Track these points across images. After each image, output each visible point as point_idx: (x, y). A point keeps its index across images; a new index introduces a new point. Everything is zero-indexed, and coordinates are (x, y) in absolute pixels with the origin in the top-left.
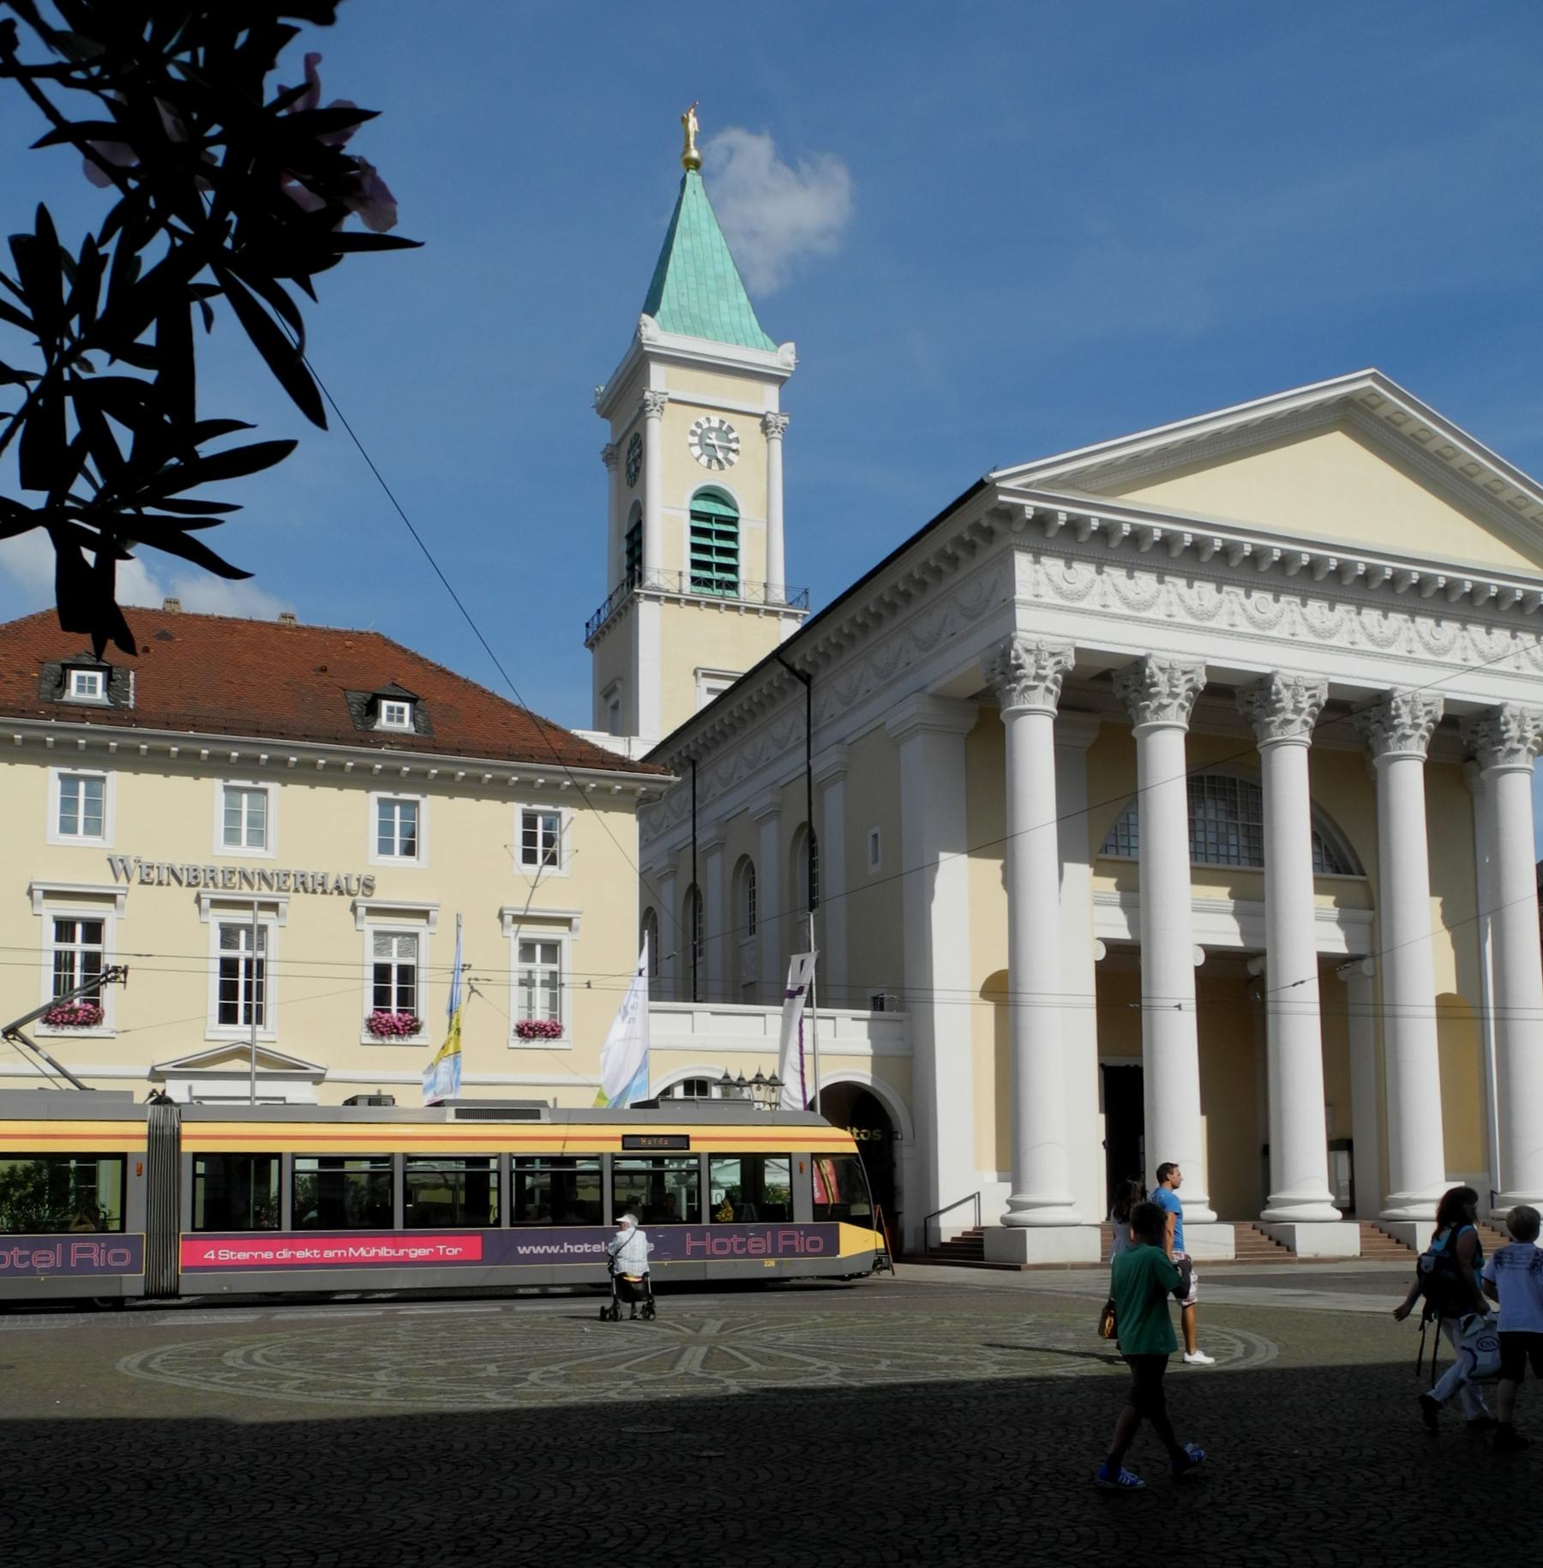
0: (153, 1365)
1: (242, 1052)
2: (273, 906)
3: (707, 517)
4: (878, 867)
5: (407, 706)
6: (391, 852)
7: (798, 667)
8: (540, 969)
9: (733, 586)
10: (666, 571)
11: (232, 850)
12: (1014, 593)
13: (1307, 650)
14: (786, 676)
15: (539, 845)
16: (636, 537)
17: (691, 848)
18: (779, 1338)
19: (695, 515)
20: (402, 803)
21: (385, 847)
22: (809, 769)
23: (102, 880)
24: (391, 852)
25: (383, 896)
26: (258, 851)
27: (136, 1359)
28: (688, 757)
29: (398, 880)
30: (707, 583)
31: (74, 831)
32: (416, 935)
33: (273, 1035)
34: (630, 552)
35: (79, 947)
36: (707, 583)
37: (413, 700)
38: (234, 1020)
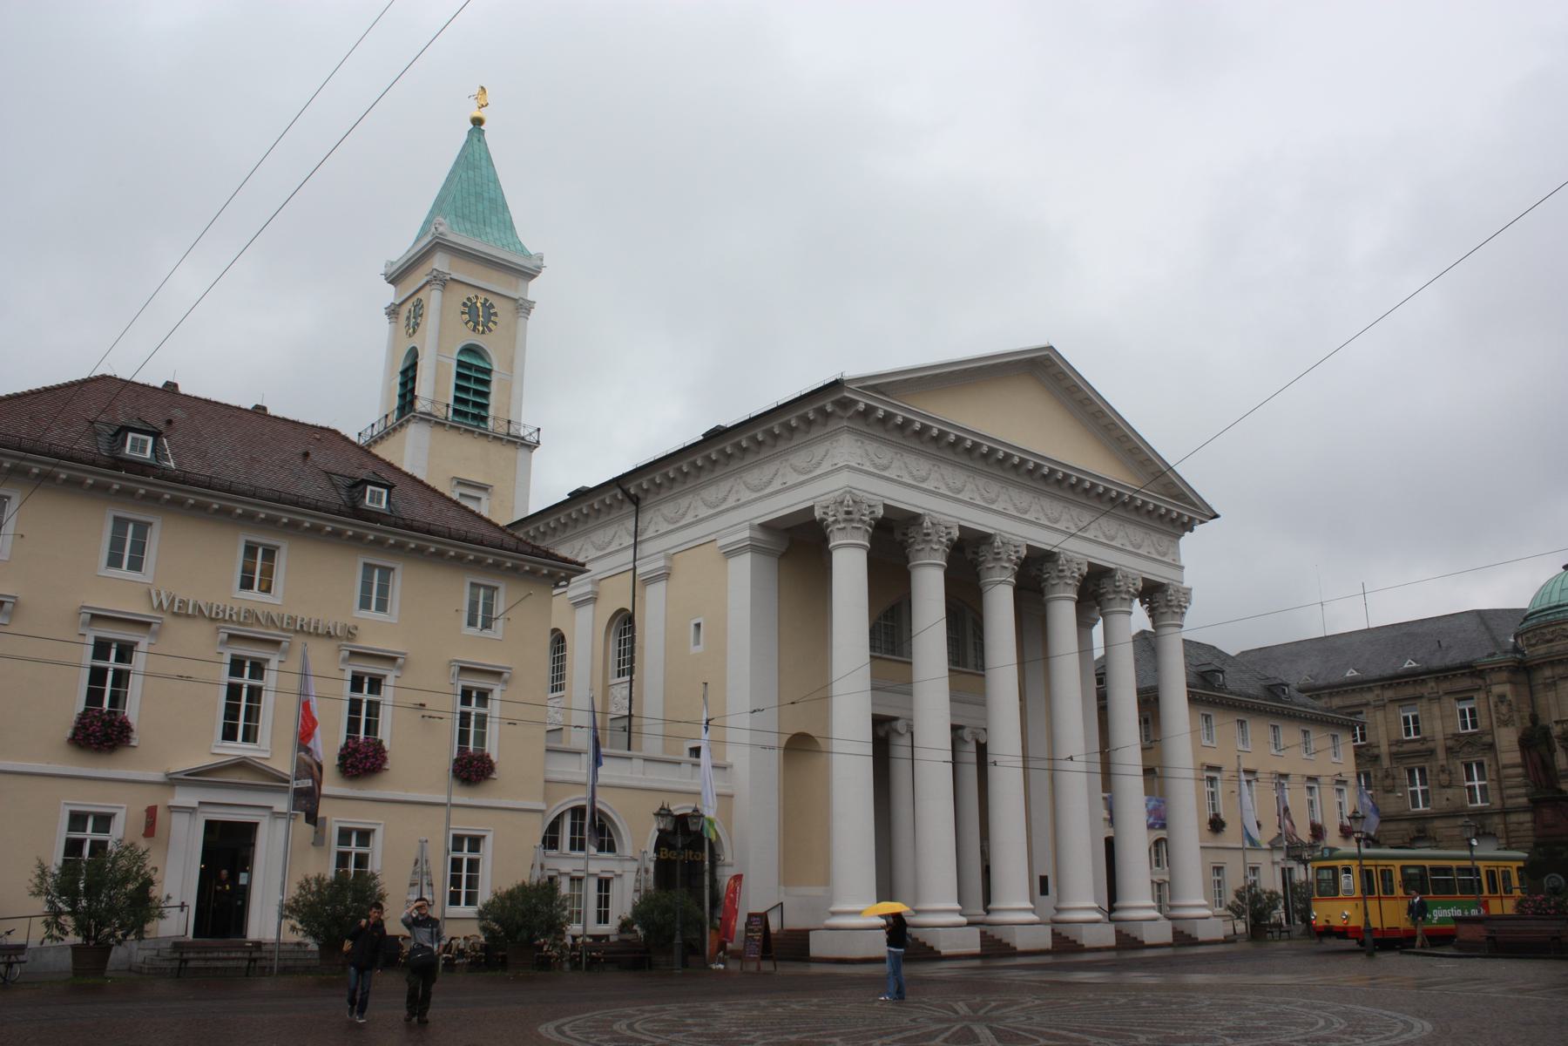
0: (1401, 1026)
1: (242, 765)
3: (469, 366)
4: (700, 649)
5: (385, 492)
7: (632, 491)
8: (473, 709)
9: (484, 419)
12: (329, 436)
13: (1017, 522)
16: (410, 374)
19: (460, 364)
21: (365, 604)
22: (634, 568)
23: (139, 609)
25: (366, 642)
26: (265, 597)
27: (551, 1026)
30: (465, 415)
31: (119, 566)
36: (465, 415)
37: (390, 488)
38: (234, 738)
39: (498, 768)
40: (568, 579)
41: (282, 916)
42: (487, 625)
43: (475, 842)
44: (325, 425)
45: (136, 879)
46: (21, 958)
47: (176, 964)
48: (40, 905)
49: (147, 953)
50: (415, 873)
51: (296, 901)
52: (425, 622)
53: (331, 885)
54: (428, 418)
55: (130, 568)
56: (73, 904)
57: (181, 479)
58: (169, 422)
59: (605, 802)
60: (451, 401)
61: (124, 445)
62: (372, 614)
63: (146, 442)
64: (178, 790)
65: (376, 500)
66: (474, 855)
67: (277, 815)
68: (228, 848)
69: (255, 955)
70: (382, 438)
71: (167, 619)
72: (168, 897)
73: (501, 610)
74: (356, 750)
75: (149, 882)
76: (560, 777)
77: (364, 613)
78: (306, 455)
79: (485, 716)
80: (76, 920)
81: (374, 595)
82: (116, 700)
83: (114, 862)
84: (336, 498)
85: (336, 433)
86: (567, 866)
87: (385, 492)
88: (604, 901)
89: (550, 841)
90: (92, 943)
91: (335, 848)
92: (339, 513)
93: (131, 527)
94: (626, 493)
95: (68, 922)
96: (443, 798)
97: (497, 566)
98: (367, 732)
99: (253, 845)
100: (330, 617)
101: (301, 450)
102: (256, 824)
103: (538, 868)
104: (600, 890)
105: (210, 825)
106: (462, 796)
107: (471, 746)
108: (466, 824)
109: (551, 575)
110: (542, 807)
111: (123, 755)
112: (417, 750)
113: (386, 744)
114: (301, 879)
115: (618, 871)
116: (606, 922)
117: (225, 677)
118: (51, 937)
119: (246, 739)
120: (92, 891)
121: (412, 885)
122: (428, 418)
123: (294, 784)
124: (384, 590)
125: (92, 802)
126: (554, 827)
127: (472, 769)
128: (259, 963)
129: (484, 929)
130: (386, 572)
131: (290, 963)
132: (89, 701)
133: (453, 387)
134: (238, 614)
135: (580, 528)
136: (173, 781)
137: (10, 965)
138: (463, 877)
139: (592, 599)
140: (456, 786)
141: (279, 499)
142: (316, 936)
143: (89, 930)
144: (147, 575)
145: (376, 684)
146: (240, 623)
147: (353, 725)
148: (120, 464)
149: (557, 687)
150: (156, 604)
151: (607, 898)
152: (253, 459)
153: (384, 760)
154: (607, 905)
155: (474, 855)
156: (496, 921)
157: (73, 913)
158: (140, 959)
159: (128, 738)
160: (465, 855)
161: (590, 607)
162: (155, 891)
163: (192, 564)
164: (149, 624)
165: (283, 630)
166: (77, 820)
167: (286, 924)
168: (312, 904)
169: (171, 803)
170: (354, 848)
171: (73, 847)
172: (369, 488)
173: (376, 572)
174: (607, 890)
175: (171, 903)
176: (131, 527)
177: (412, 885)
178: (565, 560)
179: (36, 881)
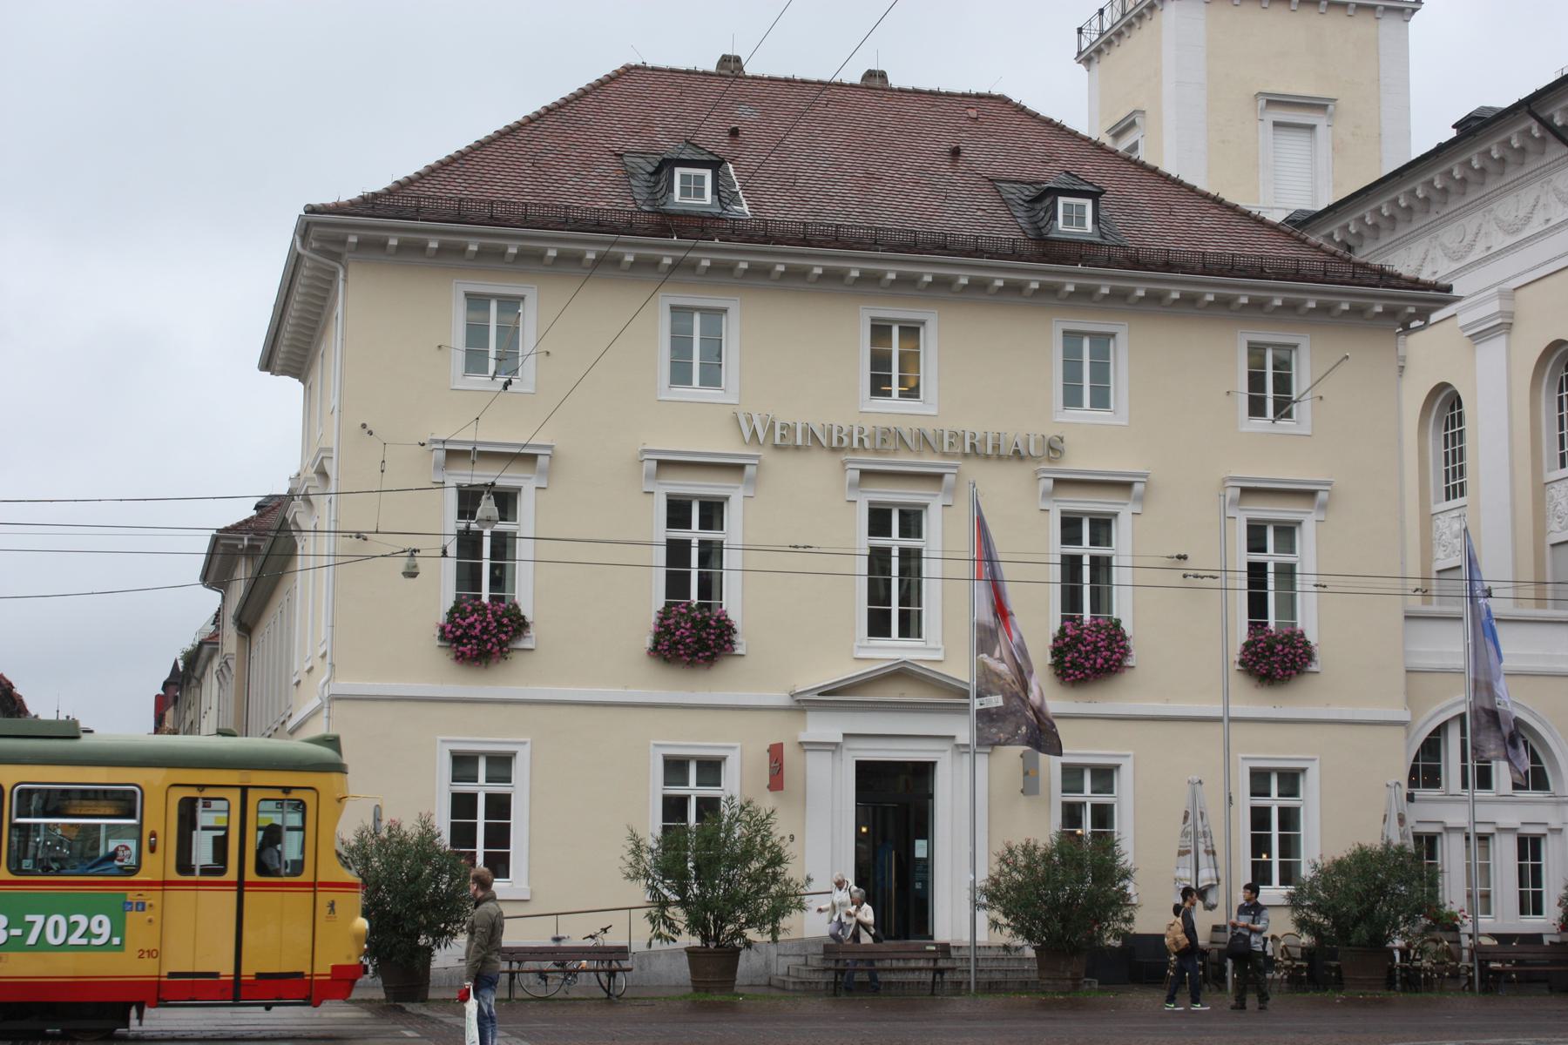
1: (901, 673)
5: (1088, 203)
6: (1079, 404)
8: (895, 542)
11: (881, 403)
14: (1536, 133)
15: (1270, 391)
20: (703, 311)
21: (1072, 398)
23: (724, 446)
24: (1079, 404)
25: (1078, 463)
26: (909, 405)
29: (1097, 441)
35: (694, 534)
37: (1095, 196)
39: (1320, 654)
40: (1423, 315)
41: (976, 905)
42: (1283, 408)
43: (1291, 781)
44: (984, 90)
45: (761, 853)
46: (625, 965)
47: (830, 977)
48: (639, 893)
49: (792, 961)
50: (1185, 834)
51: (996, 883)
52: (1169, 418)
53: (1047, 857)
55: (703, 383)
56: (682, 890)
57: (762, 235)
58: (734, 133)
59: (1514, 701)
61: (671, 188)
62: (1086, 415)
63: (701, 178)
64: (811, 717)
65: (1074, 220)
66: (1289, 802)
67: (961, 748)
68: (894, 804)
69: (941, 964)
70: (1119, 34)
71: (766, 455)
72: (809, 880)
73: (1306, 384)
74: (1077, 640)
75: (777, 860)
76: (1435, 663)
77: (1073, 415)
78: (956, 152)
79: (1292, 567)
80: (688, 913)
81: (1087, 382)
82: (707, 588)
83: (729, 830)
84: (1008, 229)
85: (1003, 101)
86: (1456, 816)
87: (1088, 203)
88: (1530, 875)
89: (1425, 772)
90: (712, 945)
91: (1058, 798)
92: (1015, 255)
94: (1547, 125)
95: (678, 915)
96: (1216, 710)
97: (1291, 307)
98: (1095, 608)
99: (932, 796)
101: (946, 145)
102: (933, 764)
103: (1394, 820)
104: (1522, 856)
105: (866, 771)
106: (1252, 702)
107: (1272, 620)
108: (1277, 752)
109: (1390, 313)
110: (1405, 716)
111: (726, 670)
112: (1181, 636)
113: (1127, 626)
114: (1000, 848)
115: (1555, 824)
116: (1538, 911)
117: (864, 542)
118: (659, 936)
119: (905, 632)
120: (706, 869)
121: (1182, 853)
123: (976, 704)
124: (1101, 372)
125: (694, 742)
126: (1432, 746)
127: (1275, 659)
128: (947, 976)
129: (1302, 924)
130: (1102, 341)
131: (998, 977)
132: (670, 592)
135: (1473, 194)
136: (802, 705)
137: (612, 974)
138: (1272, 832)
139: (1504, 326)
140: (1241, 684)
141: (913, 246)
142: (1029, 936)
143: (706, 928)
144: (728, 393)
145: (1102, 527)
146: (876, 451)
147: (1071, 600)
148: (670, 224)
149: (1455, 491)
150: (747, 435)
151: (1537, 870)
152: (869, 176)
153: (1126, 652)
154: (1537, 881)
155: (1289, 802)
156: (1315, 908)
157: (683, 903)
158: (782, 970)
159: (731, 642)
160: (1274, 802)
161: (1503, 339)
162: (791, 871)
163: (793, 361)
164: (741, 467)
165: (944, 455)
166: (675, 768)
167: (983, 917)
168: (1019, 888)
169: (804, 738)
170: (1088, 796)
171: (674, 808)
172: (1061, 201)
173: (1086, 343)
174: (1537, 855)
175: (813, 888)
177: (1182, 853)
178: (1415, 284)
179: (631, 858)
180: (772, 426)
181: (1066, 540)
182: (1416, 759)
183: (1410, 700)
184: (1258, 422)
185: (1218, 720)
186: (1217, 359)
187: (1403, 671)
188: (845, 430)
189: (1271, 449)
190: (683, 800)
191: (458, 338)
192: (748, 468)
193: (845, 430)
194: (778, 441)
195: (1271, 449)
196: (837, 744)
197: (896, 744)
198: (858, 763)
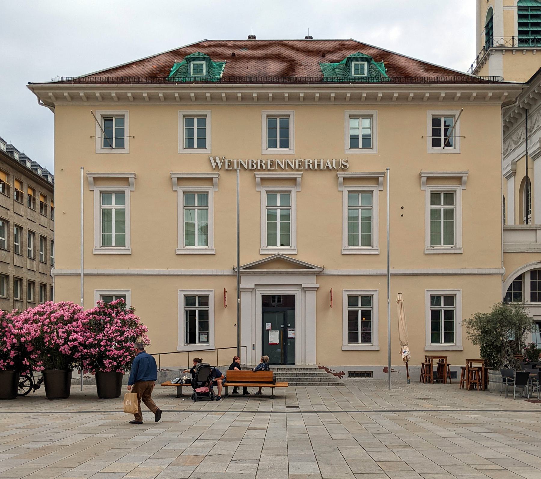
1: (279, 260)
2: (293, 180)
8: (442, 207)
10: (506, 37)
11: (272, 151)
16: (490, 26)
17: (525, 157)
18: (199, 361)
23: (204, 169)
24: (358, 146)
25: (355, 169)
26: (284, 151)
28: (523, 108)
30: (527, 41)
32: (372, 192)
33: (296, 251)
34: (487, 34)
35: (442, 207)
36: (527, 41)
54: (503, 50)
55: (363, 146)
60: (516, 34)
71: (222, 173)
77: (354, 151)
87: (365, 63)
89: (514, 292)
91: (346, 308)
93: (196, 120)
96: (383, 270)
100: (329, 158)
105: (265, 299)
122: (503, 50)
126: (518, 283)
133: (516, 25)
134: (266, 164)
176: (196, 120)
180: (224, 162)
181: (432, 203)
182: (510, 289)
183: (504, 263)
184: (437, 150)
185: (79, 275)
186: (172, 125)
187: (500, 252)
188: (255, 162)
189: (444, 161)
190: (439, 312)
191: (99, 134)
192: (380, 179)
193: (255, 162)
194: (227, 167)
195: (444, 161)
196: (253, 288)
197: (279, 288)
198: (262, 296)
